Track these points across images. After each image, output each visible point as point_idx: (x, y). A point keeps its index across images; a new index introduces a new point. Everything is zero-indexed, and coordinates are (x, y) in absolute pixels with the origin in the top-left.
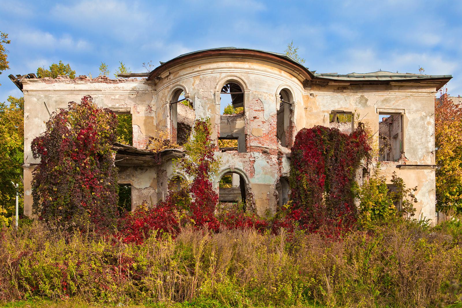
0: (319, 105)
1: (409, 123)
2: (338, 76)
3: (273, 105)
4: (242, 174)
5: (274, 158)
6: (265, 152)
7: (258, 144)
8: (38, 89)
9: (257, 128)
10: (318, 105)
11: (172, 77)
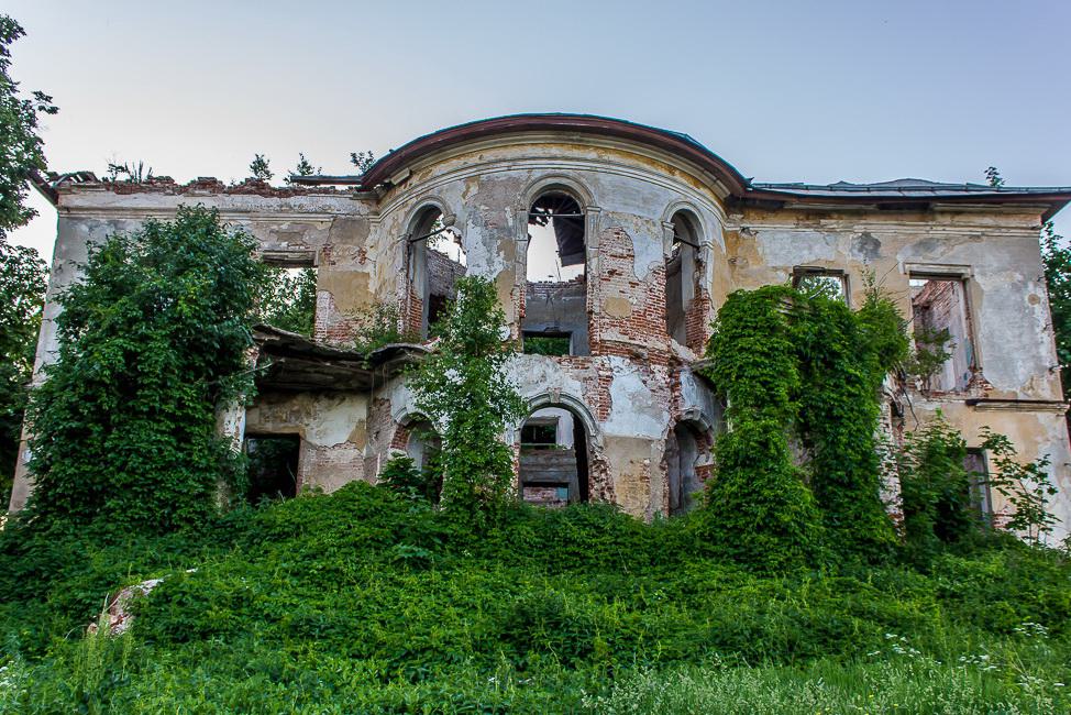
0: (764, 254)
1: (985, 297)
2: (807, 188)
3: (653, 252)
4: (581, 410)
5: (660, 373)
6: (635, 357)
7: (619, 335)
8: (95, 205)
9: (617, 296)
10: (760, 253)
11: (415, 180)
